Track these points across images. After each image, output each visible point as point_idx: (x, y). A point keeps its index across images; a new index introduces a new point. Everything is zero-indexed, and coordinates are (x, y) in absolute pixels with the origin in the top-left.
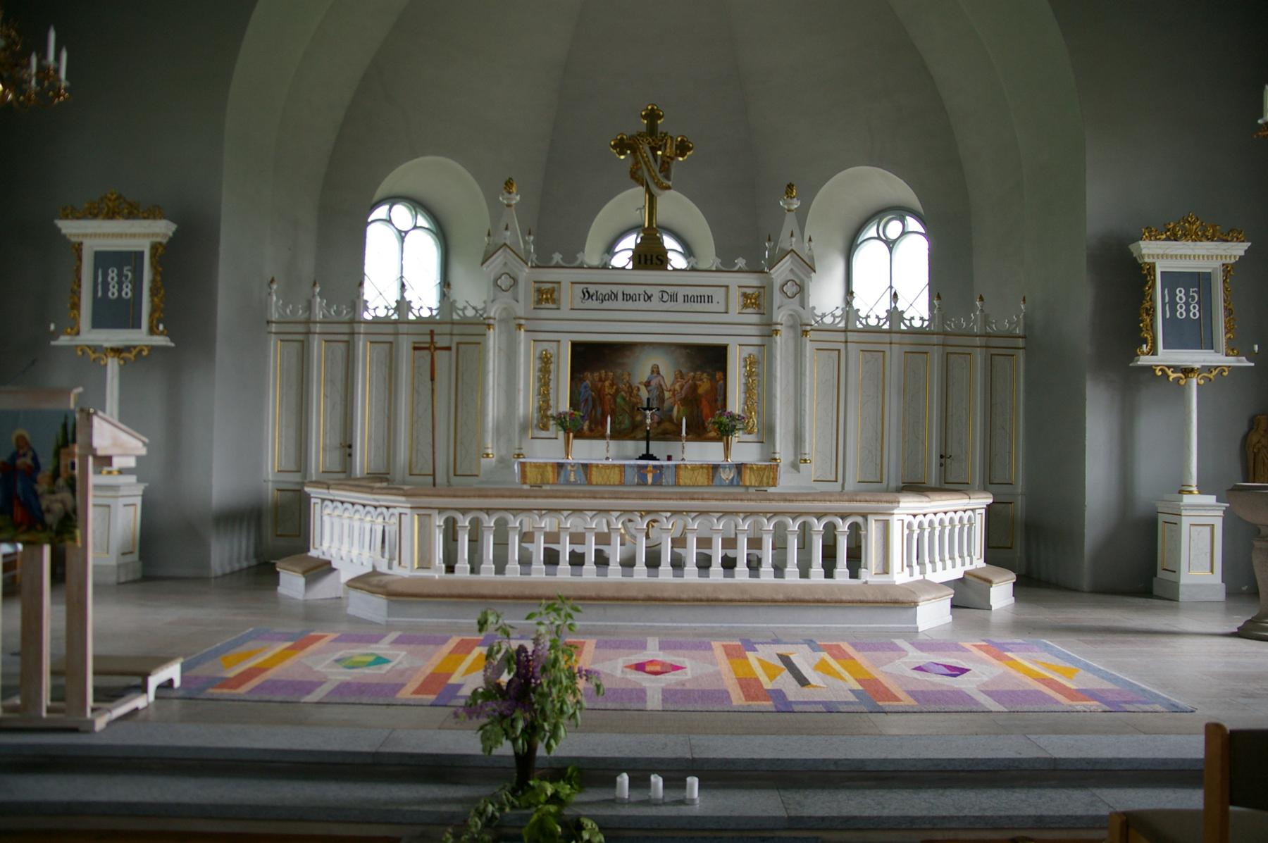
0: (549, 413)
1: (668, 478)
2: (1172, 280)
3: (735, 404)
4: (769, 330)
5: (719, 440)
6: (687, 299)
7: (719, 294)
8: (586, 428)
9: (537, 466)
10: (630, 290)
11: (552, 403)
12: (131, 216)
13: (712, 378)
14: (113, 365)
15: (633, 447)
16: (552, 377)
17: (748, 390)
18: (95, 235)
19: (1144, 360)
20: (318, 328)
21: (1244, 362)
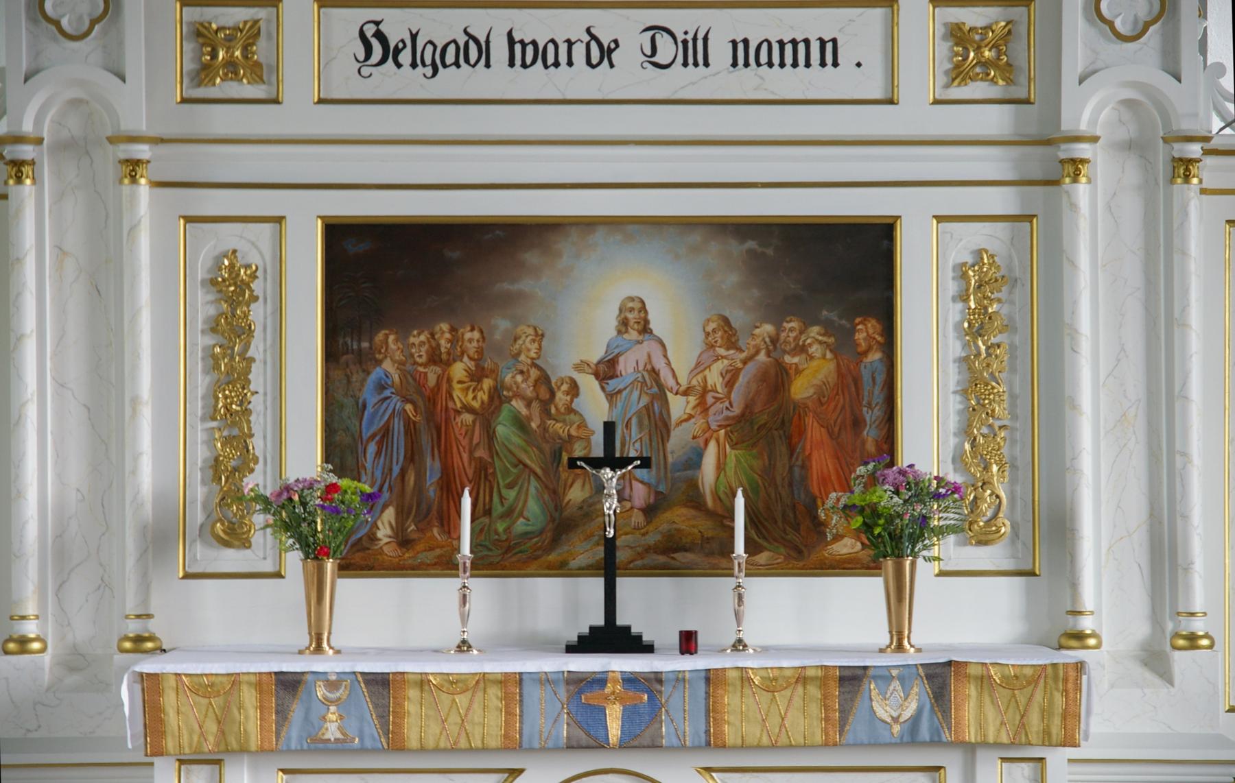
0: (250, 482)
1: (682, 715)
3: (927, 438)
4: (1050, 163)
5: (869, 567)
8: (384, 532)
9: (204, 687)
11: (257, 445)
13: (842, 343)
16: (257, 349)
17: (976, 385)
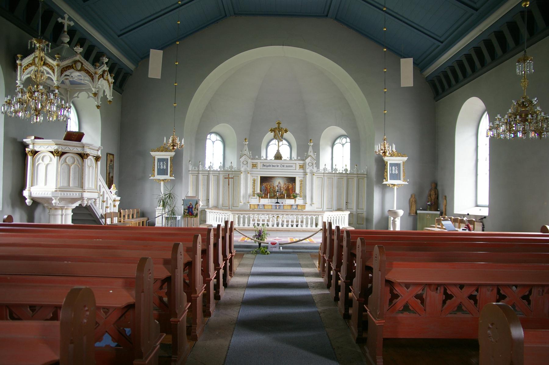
1: (282, 208)
2: (391, 165)
3: (297, 191)
4: (305, 174)
6: (287, 166)
7: (294, 165)
10: (274, 164)
12: (166, 151)
13: (292, 185)
14: (162, 183)
15: (274, 200)
17: (301, 187)
18: (158, 155)
19: (385, 183)
20: (201, 172)
21: (406, 183)
